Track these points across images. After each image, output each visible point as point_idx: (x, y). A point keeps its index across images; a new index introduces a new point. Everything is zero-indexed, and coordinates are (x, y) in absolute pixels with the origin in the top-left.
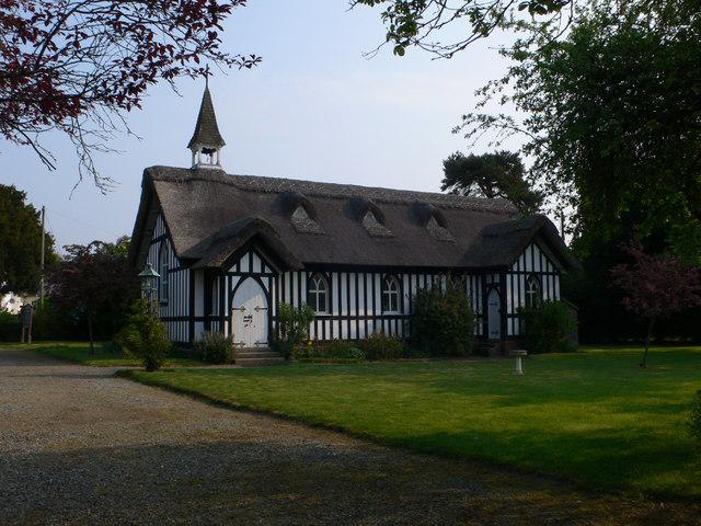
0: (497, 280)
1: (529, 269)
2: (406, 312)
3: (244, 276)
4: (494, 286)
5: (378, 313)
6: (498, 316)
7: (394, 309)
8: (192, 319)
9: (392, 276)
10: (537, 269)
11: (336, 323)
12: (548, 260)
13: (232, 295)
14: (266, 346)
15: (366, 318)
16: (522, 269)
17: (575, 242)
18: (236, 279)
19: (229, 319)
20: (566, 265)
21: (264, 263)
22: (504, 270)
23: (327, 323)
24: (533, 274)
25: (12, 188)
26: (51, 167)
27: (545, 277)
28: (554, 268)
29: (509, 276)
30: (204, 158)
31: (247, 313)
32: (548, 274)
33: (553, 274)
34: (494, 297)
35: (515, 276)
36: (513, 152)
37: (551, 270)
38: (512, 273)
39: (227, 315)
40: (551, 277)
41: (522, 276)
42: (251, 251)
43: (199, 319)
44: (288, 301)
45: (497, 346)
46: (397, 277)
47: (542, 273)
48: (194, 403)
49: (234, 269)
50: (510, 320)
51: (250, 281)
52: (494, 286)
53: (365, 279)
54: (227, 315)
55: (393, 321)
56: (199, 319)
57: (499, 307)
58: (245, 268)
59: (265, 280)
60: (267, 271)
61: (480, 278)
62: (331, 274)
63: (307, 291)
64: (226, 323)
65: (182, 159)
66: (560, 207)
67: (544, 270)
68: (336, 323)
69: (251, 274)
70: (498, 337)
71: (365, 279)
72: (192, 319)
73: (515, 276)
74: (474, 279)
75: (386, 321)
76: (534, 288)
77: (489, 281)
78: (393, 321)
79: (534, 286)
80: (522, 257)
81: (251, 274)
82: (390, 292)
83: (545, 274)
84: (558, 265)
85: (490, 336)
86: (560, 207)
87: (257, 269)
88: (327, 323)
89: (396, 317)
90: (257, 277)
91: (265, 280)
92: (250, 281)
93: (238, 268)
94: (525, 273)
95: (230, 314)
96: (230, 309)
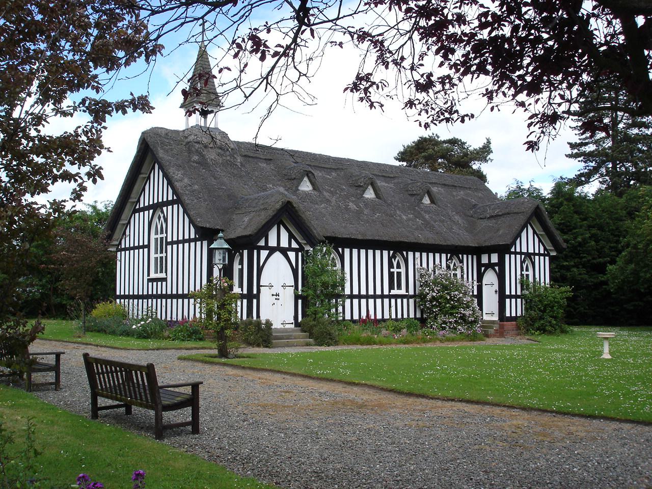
0: (495, 258)
1: (524, 250)
2: (411, 292)
3: (272, 250)
4: (490, 266)
5: (386, 292)
6: (496, 297)
10: (531, 251)
12: (540, 241)
14: (293, 326)
15: (103, 373)
17: (567, 14)
19: (258, 296)
20: (441, 143)
21: (291, 236)
22: (504, 250)
24: (528, 255)
26: (49, 123)
27: (537, 257)
28: (545, 249)
29: (507, 256)
32: (539, 255)
33: (544, 255)
34: (490, 278)
36: (465, 77)
37: (542, 252)
38: (510, 253)
39: (255, 292)
40: (542, 258)
42: (280, 223)
44: (425, 265)
45: (496, 327)
46: (403, 255)
47: (535, 254)
49: (262, 243)
50: (508, 301)
51: (277, 255)
52: (490, 266)
53: (171, 318)
54: (255, 292)
57: (496, 287)
58: (273, 243)
59: (292, 255)
60: (294, 245)
61: (475, 257)
62: (343, 251)
63: (389, 270)
64: (255, 301)
67: (537, 251)
69: (279, 249)
70: (496, 318)
71: (171, 318)
75: (393, 301)
78: (399, 301)
80: (518, 242)
81: (279, 249)
82: (395, 270)
83: (537, 254)
84: (550, 247)
87: (284, 243)
90: (284, 252)
91: (292, 255)
92: (277, 255)
93: (267, 242)
94: (521, 253)
96: (259, 286)
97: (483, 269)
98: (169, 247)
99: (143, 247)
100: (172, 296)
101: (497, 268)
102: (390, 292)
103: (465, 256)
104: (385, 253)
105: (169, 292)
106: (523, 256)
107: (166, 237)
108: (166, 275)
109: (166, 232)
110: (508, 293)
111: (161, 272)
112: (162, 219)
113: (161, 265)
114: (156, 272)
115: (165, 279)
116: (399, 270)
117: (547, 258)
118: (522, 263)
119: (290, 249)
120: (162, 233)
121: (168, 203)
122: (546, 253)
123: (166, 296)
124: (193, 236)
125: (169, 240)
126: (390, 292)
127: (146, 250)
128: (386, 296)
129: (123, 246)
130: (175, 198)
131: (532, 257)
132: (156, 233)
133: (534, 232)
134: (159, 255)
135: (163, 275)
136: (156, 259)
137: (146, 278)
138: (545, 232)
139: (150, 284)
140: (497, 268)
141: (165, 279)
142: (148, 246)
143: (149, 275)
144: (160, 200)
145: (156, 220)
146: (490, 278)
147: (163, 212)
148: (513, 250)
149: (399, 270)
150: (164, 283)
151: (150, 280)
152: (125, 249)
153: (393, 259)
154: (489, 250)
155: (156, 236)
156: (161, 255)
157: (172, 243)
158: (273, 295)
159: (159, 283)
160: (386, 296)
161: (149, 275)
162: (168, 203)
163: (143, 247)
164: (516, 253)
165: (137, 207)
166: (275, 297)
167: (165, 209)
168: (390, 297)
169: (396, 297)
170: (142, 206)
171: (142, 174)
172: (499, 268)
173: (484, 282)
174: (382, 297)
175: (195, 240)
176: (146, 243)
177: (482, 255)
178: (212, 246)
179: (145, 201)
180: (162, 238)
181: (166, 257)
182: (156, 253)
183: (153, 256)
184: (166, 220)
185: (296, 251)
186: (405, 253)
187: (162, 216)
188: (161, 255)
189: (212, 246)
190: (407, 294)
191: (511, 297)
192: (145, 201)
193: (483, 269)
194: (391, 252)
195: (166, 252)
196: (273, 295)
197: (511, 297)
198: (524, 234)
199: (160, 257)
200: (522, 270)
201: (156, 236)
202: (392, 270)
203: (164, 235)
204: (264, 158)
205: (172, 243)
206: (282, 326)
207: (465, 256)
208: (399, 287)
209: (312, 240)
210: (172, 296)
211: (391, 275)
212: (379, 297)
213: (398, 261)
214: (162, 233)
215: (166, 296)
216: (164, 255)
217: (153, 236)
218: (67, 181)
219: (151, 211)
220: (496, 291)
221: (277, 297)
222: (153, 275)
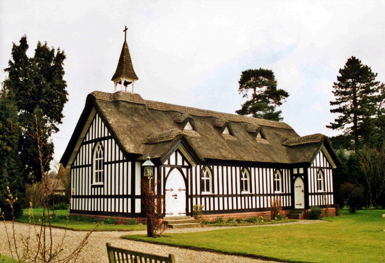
0: (301, 171)
1: (318, 166)
3: (172, 168)
4: (299, 175)
5: (239, 193)
6: (303, 195)
7: (208, 190)
8: (133, 197)
9: (207, 167)
10: (322, 166)
11: (216, 199)
13: (165, 180)
14: (185, 215)
16: (315, 166)
18: (168, 169)
19: (164, 197)
21: (184, 159)
22: (306, 165)
23: (212, 199)
24: (321, 168)
25: (36, 50)
27: (325, 170)
28: (330, 165)
29: (309, 169)
30: (121, 88)
31: (174, 193)
32: (327, 168)
33: (329, 168)
34: (299, 182)
35: (312, 169)
37: (328, 166)
38: (311, 168)
39: (162, 194)
41: (315, 169)
43: (138, 197)
47: (324, 168)
48: (246, 251)
49: (166, 163)
50: (310, 196)
51: (175, 170)
52: (299, 175)
53: (227, 169)
54: (162, 194)
55: (207, 199)
56: (138, 197)
58: (173, 162)
59: (184, 170)
60: (186, 164)
62: (213, 167)
65: (110, 87)
66: (349, 111)
67: (325, 166)
68: (216, 199)
70: (303, 207)
71: (227, 169)
72: (133, 197)
73: (312, 169)
74: (286, 170)
76: (246, 177)
77: (295, 171)
78: (207, 199)
79: (207, 173)
80: (315, 162)
81: (176, 166)
85: (296, 207)
86: (349, 111)
87: (180, 163)
88: (212, 199)
89: (209, 196)
91: (184, 170)
92: (175, 170)
94: (316, 167)
95: (164, 193)
96: (164, 190)
97: (294, 177)
98: (106, 166)
99: (89, 165)
100: (107, 197)
101: (303, 177)
102: (241, 192)
103: (284, 170)
104: (238, 168)
105: (113, 194)
106: (318, 169)
107: (104, 160)
108: (104, 183)
109: (104, 156)
110: (310, 192)
111: (100, 181)
112: (100, 148)
113: (100, 177)
114: (97, 181)
115: (103, 186)
116: (278, 180)
117: (331, 170)
118: (317, 173)
119: (183, 166)
120: (100, 157)
121: (104, 138)
122: (330, 167)
123: (104, 197)
124: (121, 159)
125: (106, 161)
126: (241, 192)
127: (90, 168)
128: (239, 195)
129: (75, 165)
130: (110, 135)
131: (323, 169)
132: (97, 157)
133: (324, 155)
134: (98, 171)
135: (101, 183)
136: (97, 173)
137: (90, 185)
138: (330, 154)
139: (93, 189)
140: (303, 177)
141: (103, 186)
142: (92, 165)
143: (92, 183)
144: (97, 137)
145: (96, 149)
146: (299, 182)
147: (101, 144)
148: (312, 166)
149: (278, 180)
150: (102, 188)
151: (92, 187)
152: (77, 167)
153: (203, 171)
154: (298, 166)
155: (97, 159)
156: (100, 171)
157: (108, 163)
158: (173, 196)
159: (99, 189)
160: (239, 195)
161: (92, 183)
162: (104, 138)
163: (89, 165)
164: (314, 167)
165: (85, 141)
166: (174, 197)
167: (103, 142)
168: (241, 196)
169: (245, 196)
170: (87, 140)
171: (88, 121)
172: (304, 177)
173: (295, 185)
174: (237, 196)
175: (123, 161)
176: (90, 163)
177: (294, 169)
178: (144, 165)
179: (89, 137)
180: (100, 161)
181: (104, 172)
182: (97, 169)
183: (95, 171)
184: (103, 149)
185: (187, 168)
186: (281, 170)
187: (100, 146)
188: (100, 171)
189: (144, 165)
190: (251, 193)
191: (312, 194)
192: (89, 137)
193: (294, 177)
194: (241, 168)
195: (104, 169)
196: (173, 196)
197: (312, 194)
198: (318, 157)
199: (245, 181)
200: (274, 177)
201: (97, 159)
202: (202, 178)
203: (102, 158)
204: (162, 110)
205: (108, 163)
206: (178, 215)
207: (284, 170)
208: (208, 190)
209: (198, 160)
210: (107, 197)
211: (241, 182)
212: (234, 196)
213: (207, 172)
214: (100, 157)
215: (104, 197)
216: (102, 170)
217: (95, 159)
218: (342, 69)
219: (94, 144)
220: (303, 191)
221: (176, 197)
222: (95, 183)
